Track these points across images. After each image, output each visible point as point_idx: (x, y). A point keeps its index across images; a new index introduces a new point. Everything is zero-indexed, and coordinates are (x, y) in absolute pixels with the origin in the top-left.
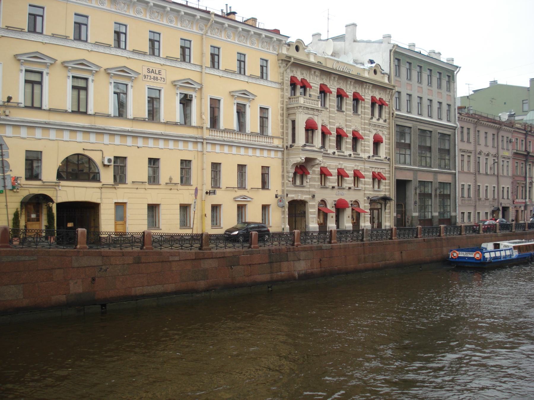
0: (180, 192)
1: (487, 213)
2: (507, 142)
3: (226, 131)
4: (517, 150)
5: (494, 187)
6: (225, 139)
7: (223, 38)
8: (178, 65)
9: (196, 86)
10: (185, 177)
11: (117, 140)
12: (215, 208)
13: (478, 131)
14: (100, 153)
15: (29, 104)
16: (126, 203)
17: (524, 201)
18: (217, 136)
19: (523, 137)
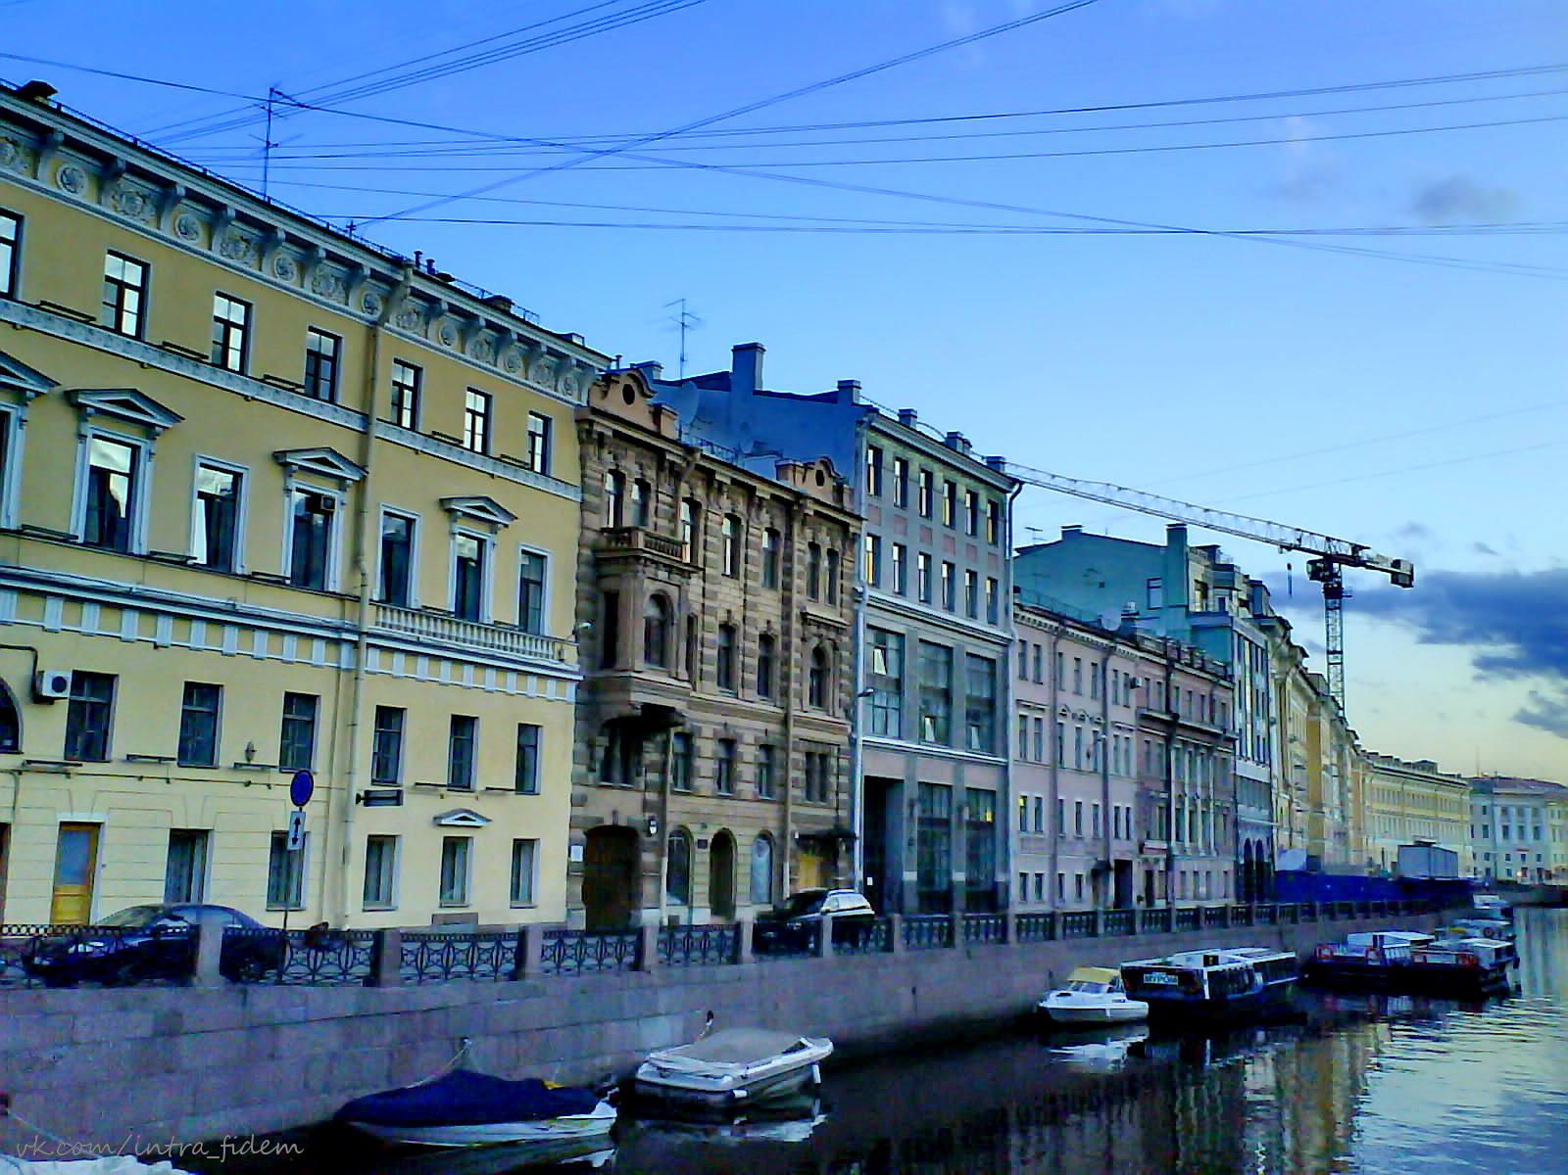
0: (178, 787)
1: (1079, 877)
2: (1125, 685)
3: (424, 613)
4: (1149, 710)
5: (1096, 806)
6: (423, 638)
7: (265, 276)
8: (297, 403)
9: (346, 473)
10: (197, 743)
11: (91, 618)
12: (379, 846)
13: (1061, 654)
16: (98, 825)
17: (1165, 846)
18: (399, 627)
19: (1159, 673)
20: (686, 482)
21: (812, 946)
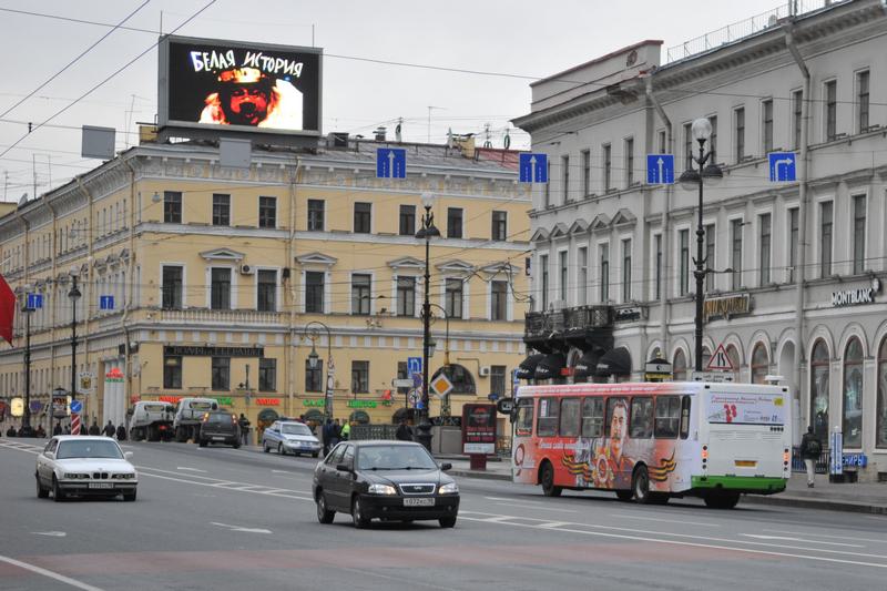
3: (192, 309)
11: (495, 347)
14: (476, 362)
15: (402, 313)
20: (16, 417)
21: (163, 428)
